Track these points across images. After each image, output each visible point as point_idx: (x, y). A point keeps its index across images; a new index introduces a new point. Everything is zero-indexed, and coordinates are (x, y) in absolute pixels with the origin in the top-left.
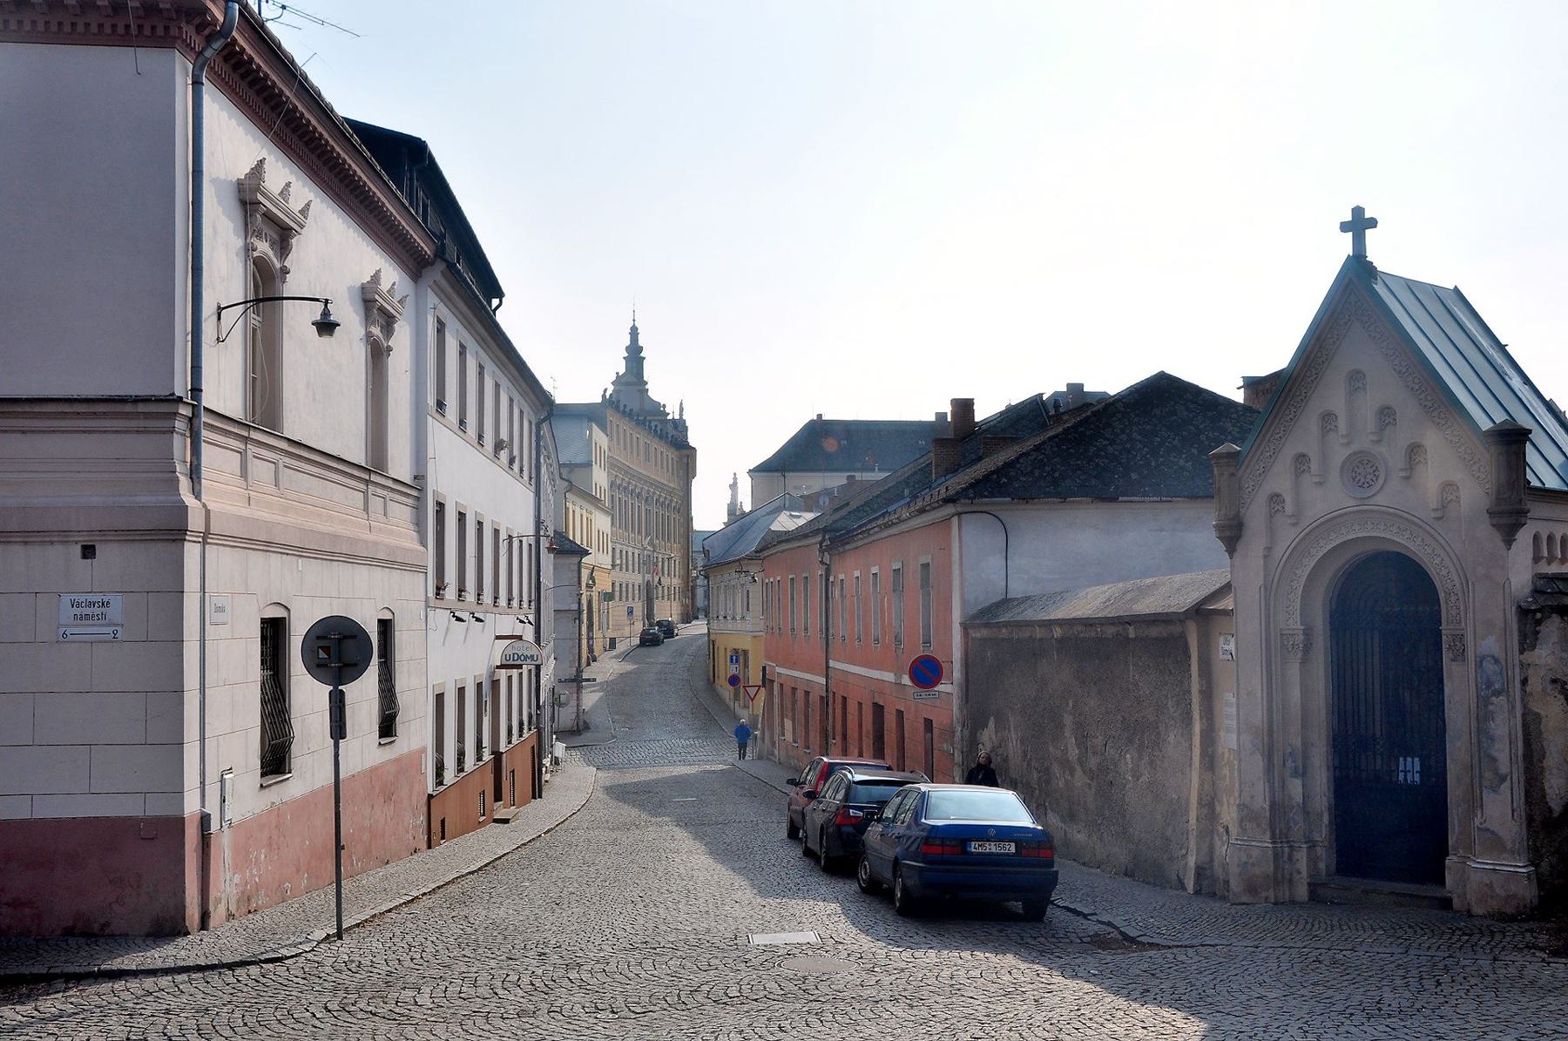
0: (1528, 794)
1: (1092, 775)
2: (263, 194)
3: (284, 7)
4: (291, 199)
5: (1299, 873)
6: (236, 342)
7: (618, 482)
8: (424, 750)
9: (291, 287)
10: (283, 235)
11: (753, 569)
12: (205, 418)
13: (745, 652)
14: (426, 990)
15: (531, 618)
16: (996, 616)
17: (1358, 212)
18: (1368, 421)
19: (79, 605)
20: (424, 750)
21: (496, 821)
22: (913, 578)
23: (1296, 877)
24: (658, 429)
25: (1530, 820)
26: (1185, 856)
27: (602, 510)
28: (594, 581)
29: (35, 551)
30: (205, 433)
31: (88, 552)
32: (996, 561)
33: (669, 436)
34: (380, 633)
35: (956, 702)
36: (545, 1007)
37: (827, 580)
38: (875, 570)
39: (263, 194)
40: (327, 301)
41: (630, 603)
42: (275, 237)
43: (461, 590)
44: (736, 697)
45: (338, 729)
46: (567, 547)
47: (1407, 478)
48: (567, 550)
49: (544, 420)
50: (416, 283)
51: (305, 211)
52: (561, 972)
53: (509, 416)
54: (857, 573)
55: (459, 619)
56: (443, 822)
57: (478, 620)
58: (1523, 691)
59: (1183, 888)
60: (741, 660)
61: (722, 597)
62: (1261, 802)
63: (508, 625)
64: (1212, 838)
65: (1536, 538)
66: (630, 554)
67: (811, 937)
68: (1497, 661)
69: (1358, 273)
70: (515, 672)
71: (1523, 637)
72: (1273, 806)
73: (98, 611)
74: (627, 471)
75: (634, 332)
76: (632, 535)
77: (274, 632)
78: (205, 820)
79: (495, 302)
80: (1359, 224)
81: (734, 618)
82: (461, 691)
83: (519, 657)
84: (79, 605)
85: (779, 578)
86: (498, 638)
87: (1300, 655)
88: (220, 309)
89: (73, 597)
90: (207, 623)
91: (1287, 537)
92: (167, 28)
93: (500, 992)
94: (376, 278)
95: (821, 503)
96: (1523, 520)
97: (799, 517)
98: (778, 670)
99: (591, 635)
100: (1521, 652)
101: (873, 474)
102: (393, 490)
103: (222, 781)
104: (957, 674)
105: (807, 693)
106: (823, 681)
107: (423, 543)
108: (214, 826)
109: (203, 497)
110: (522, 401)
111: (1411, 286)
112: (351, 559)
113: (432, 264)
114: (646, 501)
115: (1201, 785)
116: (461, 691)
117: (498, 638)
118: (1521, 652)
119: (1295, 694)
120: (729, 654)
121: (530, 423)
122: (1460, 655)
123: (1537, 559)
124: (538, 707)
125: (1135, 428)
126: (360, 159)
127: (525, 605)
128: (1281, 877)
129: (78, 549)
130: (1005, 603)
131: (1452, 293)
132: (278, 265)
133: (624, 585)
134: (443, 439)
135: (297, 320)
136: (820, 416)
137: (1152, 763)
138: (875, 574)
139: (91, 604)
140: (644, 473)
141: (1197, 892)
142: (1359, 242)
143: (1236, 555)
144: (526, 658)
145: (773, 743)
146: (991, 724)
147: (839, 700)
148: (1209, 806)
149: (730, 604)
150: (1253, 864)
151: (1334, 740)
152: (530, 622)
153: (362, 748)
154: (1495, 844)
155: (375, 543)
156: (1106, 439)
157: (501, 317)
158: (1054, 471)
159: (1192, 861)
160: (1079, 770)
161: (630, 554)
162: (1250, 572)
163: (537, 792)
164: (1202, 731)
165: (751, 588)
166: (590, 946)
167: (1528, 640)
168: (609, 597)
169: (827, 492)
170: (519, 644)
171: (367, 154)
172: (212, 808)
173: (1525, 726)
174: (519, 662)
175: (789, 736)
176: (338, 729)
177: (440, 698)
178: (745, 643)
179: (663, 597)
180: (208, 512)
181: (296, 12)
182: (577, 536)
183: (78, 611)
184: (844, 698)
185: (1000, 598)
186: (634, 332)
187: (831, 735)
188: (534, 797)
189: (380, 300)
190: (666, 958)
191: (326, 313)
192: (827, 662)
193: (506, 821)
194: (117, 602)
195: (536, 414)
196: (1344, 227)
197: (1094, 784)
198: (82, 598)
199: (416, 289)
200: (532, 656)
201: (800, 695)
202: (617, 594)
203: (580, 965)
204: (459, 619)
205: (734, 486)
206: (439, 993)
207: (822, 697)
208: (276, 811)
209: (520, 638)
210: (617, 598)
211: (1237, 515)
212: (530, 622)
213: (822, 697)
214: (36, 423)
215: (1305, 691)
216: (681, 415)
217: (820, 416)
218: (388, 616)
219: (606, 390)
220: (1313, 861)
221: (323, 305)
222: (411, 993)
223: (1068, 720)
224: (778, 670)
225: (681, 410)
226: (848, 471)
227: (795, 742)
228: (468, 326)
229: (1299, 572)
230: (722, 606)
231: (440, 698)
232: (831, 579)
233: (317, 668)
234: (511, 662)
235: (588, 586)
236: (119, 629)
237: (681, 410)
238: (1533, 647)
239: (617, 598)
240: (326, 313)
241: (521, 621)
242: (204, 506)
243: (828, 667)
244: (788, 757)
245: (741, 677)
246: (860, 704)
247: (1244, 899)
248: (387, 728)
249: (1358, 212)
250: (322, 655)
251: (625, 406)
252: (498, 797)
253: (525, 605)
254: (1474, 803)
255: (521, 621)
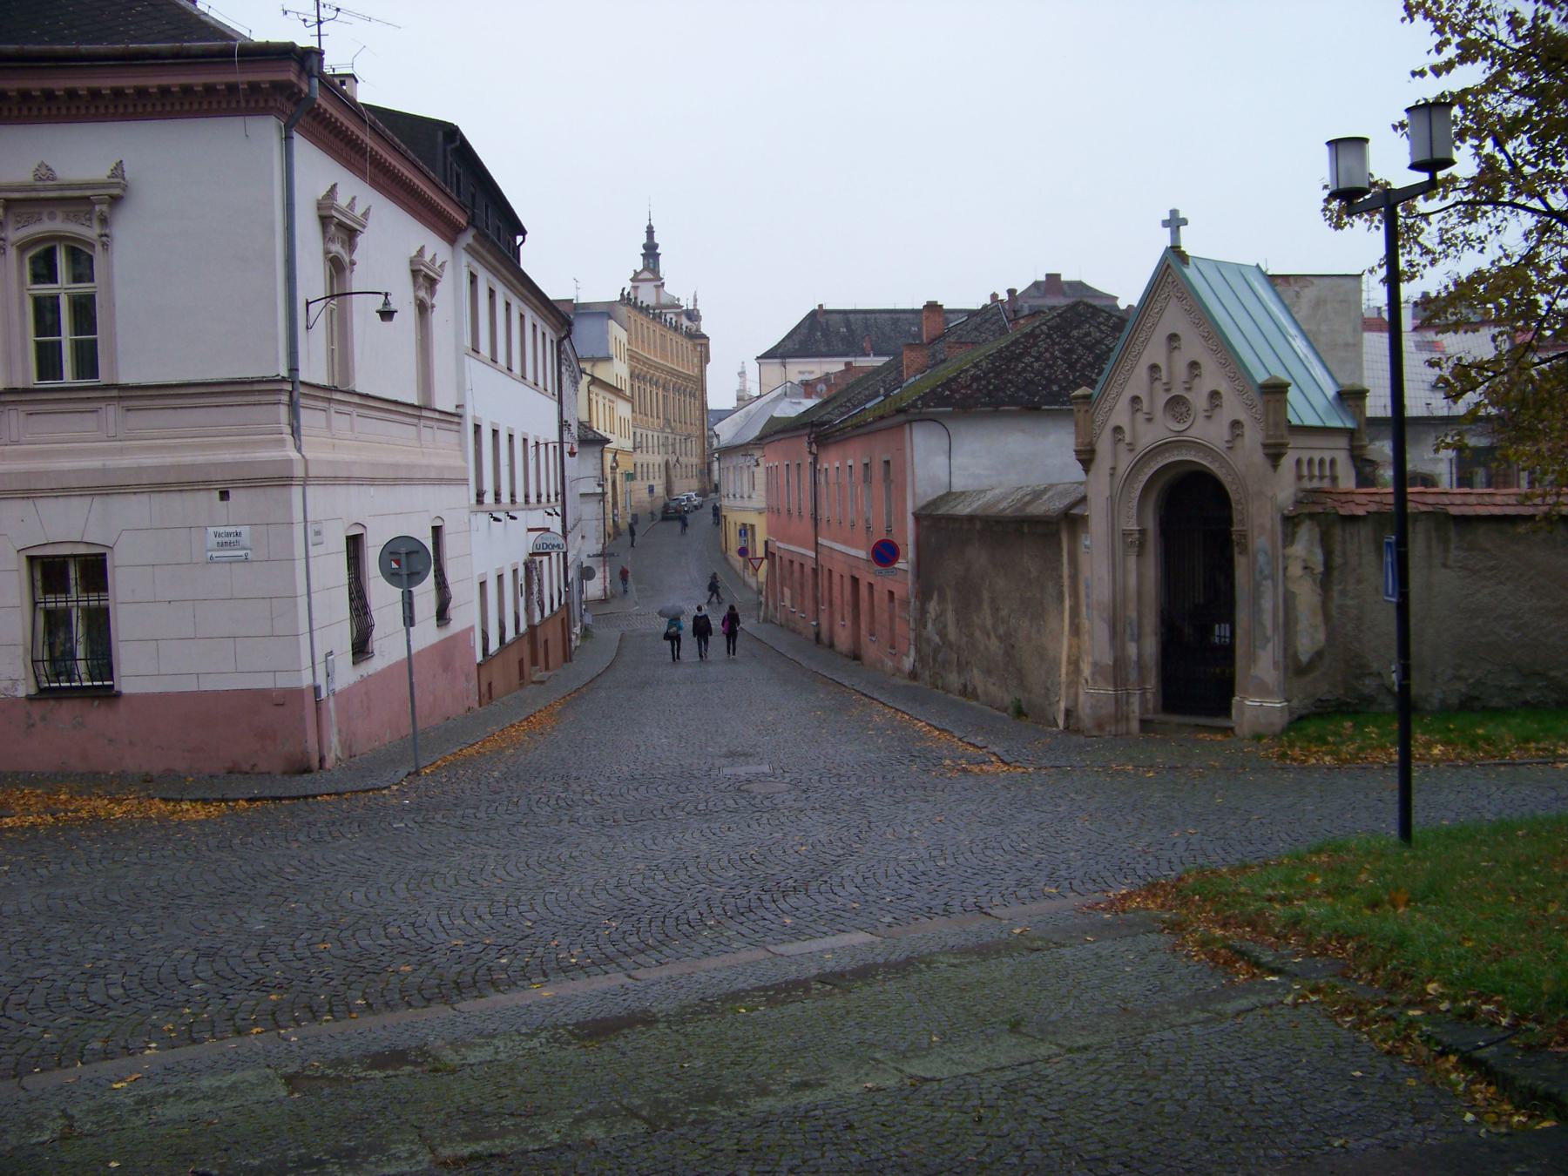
0: (1285, 649)
1: (1000, 638)
2: (336, 210)
3: (338, 10)
4: (356, 208)
5: (1133, 712)
6: (321, 326)
7: (637, 372)
8: (472, 628)
9: (357, 281)
10: (350, 234)
11: (757, 454)
12: (302, 390)
13: (752, 526)
14: (483, 808)
15: (559, 510)
16: (937, 509)
17: (1174, 213)
18: (1181, 371)
19: (220, 535)
20: (472, 628)
21: (533, 682)
22: (877, 471)
23: (1131, 715)
24: (673, 322)
25: (1286, 668)
26: (1058, 701)
27: (624, 399)
28: (617, 464)
29: (187, 496)
30: (303, 401)
31: (224, 495)
32: (941, 460)
33: (684, 327)
34: (434, 549)
35: (910, 577)
36: (566, 818)
37: (815, 468)
38: (850, 462)
39: (336, 210)
40: (386, 294)
41: (652, 482)
42: (346, 238)
43: (497, 495)
44: (746, 567)
45: (409, 620)
46: (591, 436)
47: (1208, 417)
48: (592, 441)
49: (564, 338)
50: (453, 249)
51: (366, 214)
52: (579, 796)
53: (536, 336)
54: (837, 464)
55: (496, 519)
56: (490, 684)
57: (513, 518)
58: (1284, 575)
59: (1057, 726)
60: (749, 533)
61: (731, 476)
62: (1107, 659)
63: (538, 518)
64: (1077, 688)
65: (1299, 462)
66: (650, 437)
67: (766, 768)
68: (1266, 553)
69: (1175, 255)
70: (545, 559)
71: (1285, 535)
72: (1115, 661)
73: (232, 539)
74: (645, 361)
75: (650, 231)
76: (650, 420)
77: (355, 544)
78: (317, 690)
79: (519, 239)
80: (1175, 222)
81: (742, 497)
82: (500, 577)
83: (548, 546)
84: (220, 535)
85: (777, 464)
86: (530, 530)
87: (1136, 549)
88: (308, 304)
89: (216, 529)
90: (310, 543)
91: (1125, 462)
92: (266, 101)
93: (535, 809)
94: (421, 252)
95: (818, 389)
96: (1283, 451)
97: (799, 403)
98: (778, 544)
99: (616, 512)
100: (1284, 547)
101: (868, 359)
102: (442, 421)
103: (326, 661)
104: (911, 554)
105: (802, 565)
106: (813, 554)
107: (466, 459)
108: (324, 694)
109: (303, 449)
110: (544, 324)
111: (1218, 266)
112: (409, 481)
113: (466, 229)
114: (664, 388)
115: (1070, 647)
116: (500, 577)
117: (530, 530)
118: (1284, 547)
119: (1132, 580)
120: (738, 528)
121: (552, 341)
122: (1244, 550)
123: (1300, 477)
124: (566, 584)
125: (1057, 347)
126: (407, 163)
127: (553, 499)
128: (1120, 717)
129: (216, 494)
130: (949, 496)
131: (1255, 269)
132: (347, 259)
133: (645, 466)
134: (477, 371)
135: (363, 311)
136: (821, 306)
137: (1039, 631)
138: (850, 466)
139: (228, 534)
140: (662, 362)
141: (1067, 728)
142: (1175, 234)
143: (1090, 473)
144: (553, 546)
145: (776, 609)
146: (935, 597)
147: (826, 571)
148: (1075, 664)
149: (738, 484)
150: (1101, 707)
151: (1162, 612)
152: (557, 514)
153: (427, 633)
154: (1263, 690)
155: (428, 467)
156: (1032, 356)
157: (525, 265)
158: (989, 383)
159: (1062, 705)
160: (992, 635)
161: (650, 437)
162: (1099, 489)
163: (567, 657)
164: (1071, 607)
165: (756, 470)
166: (602, 778)
167: (1289, 538)
168: (630, 477)
169: (826, 379)
170: (548, 534)
171: (412, 155)
172: (321, 680)
173: (1285, 601)
174: (548, 550)
175: (788, 603)
176: (409, 620)
177: (483, 584)
178: (751, 519)
179: (681, 476)
180: (306, 461)
181: (348, 13)
182: (601, 428)
183: (220, 540)
184: (830, 571)
185: (942, 492)
186: (650, 231)
187: (820, 601)
188: (565, 661)
189: (425, 270)
190: (655, 785)
191: (386, 303)
192: (816, 538)
193: (542, 682)
194: (245, 530)
195: (556, 332)
196: (1165, 224)
197: (1003, 646)
198: (222, 530)
199: (453, 257)
200: (558, 545)
201: (796, 566)
202: (639, 475)
203: (593, 791)
204: (496, 519)
205: (742, 374)
206: (491, 810)
207: (813, 569)
208: (364, 680)
209: (547, 530)
210: (639, 478)
211: (1091, 444)
212: (557, 514)
213: (813, 569)
214: (179, 402)
215: (1140, 576)
216: (695, 305)
217: (821, 306)
218: (438, 523)
219: (623, 289)
220: (1143, 702)
221: (384, 297)
222: (472, 811)
223: (986, 595)
224: (778, 544)
225: (695, 300)
226: (846, 355)
227: (793, 607)
228: (495, 272)
229: (1136, 486)
230: (731, 485)
231: (483, 584)
232: (818, 467)
233: (392, 577)
234: (541, 551)
235: (612, 468)
236: (248, 551)
237: (695, 300)
238: (1292, 543)
239: (639, 478)
240: (386, 303)
241: (549, 514)
242: (303, 456)
243: (817, 543)
244: (787, 620)
245: (750, 549)
246: (842, 576)
247: (1095, 733)
248: (442, 616)
249: (1174, 213)
250: (394, 565)
251: (642, 302)
252: (534, 662)
253: (553, 499)
254: (1252, 659)
255: (549, 514)
